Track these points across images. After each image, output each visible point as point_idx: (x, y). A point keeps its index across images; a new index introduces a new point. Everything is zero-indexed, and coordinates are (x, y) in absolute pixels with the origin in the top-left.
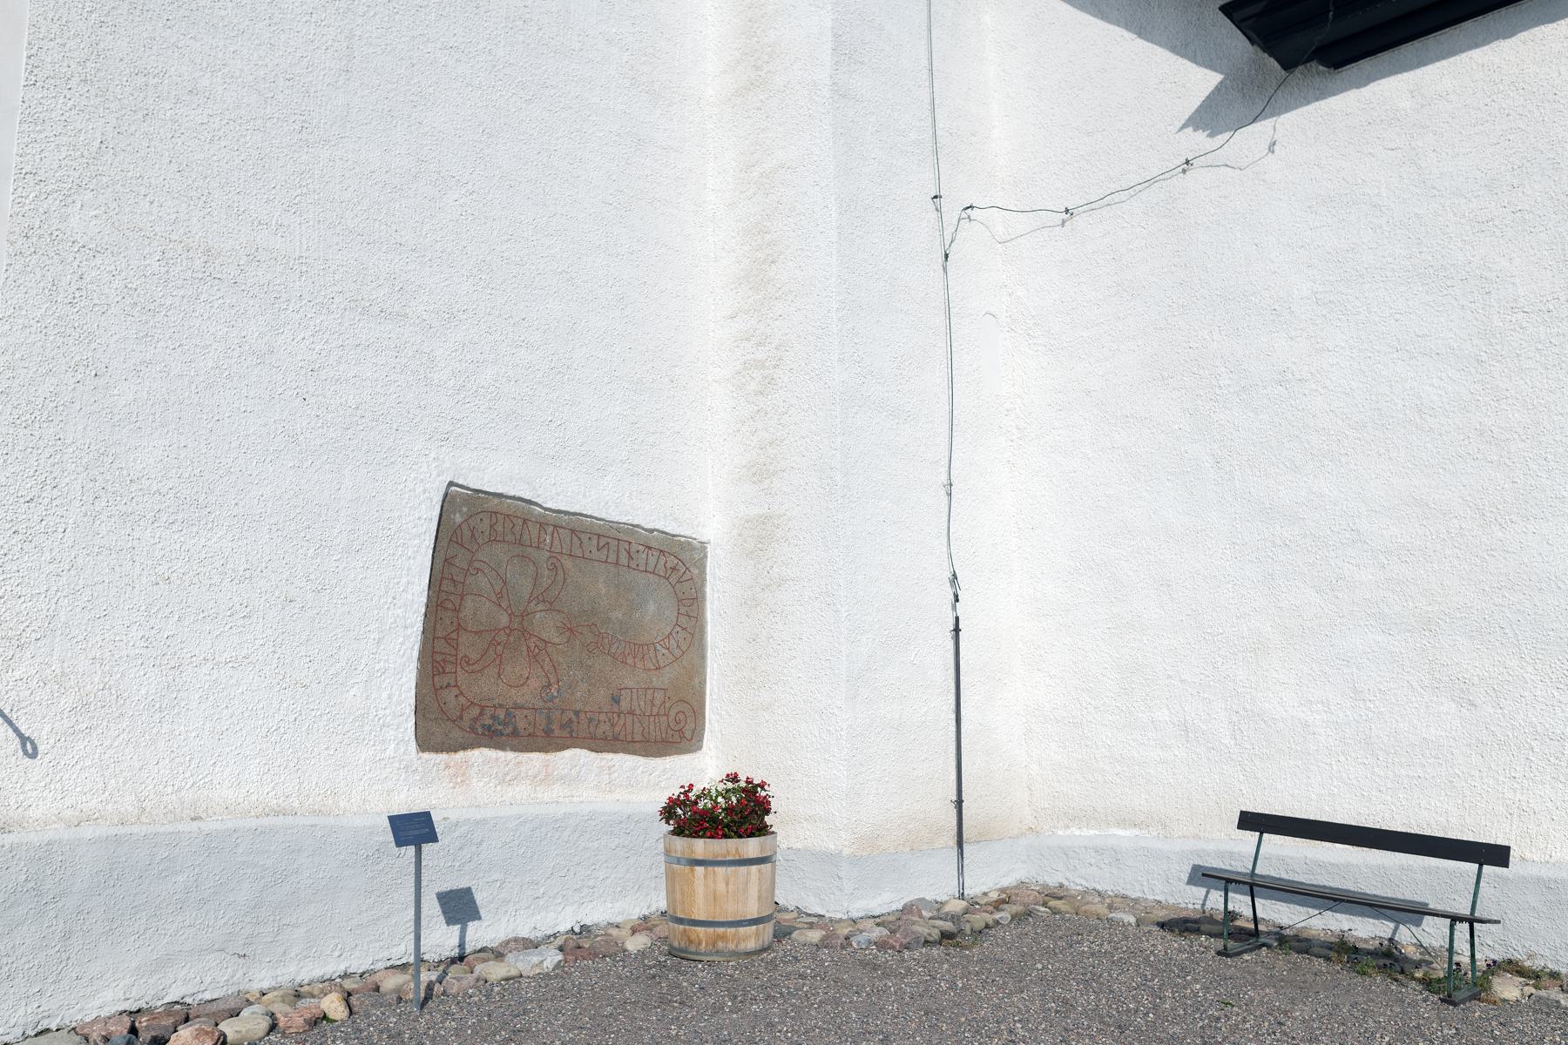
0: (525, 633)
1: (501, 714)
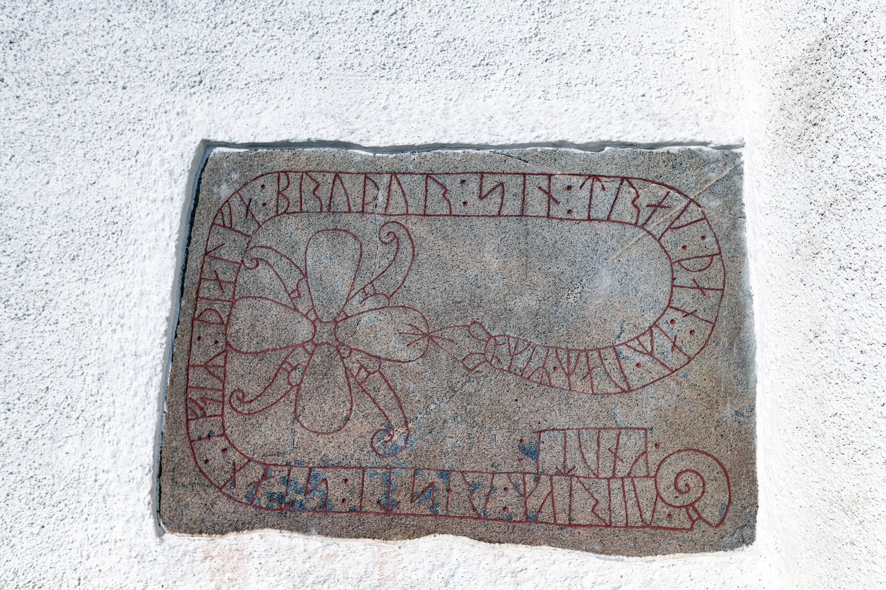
0: (340, 349)
1: (300, 476)
